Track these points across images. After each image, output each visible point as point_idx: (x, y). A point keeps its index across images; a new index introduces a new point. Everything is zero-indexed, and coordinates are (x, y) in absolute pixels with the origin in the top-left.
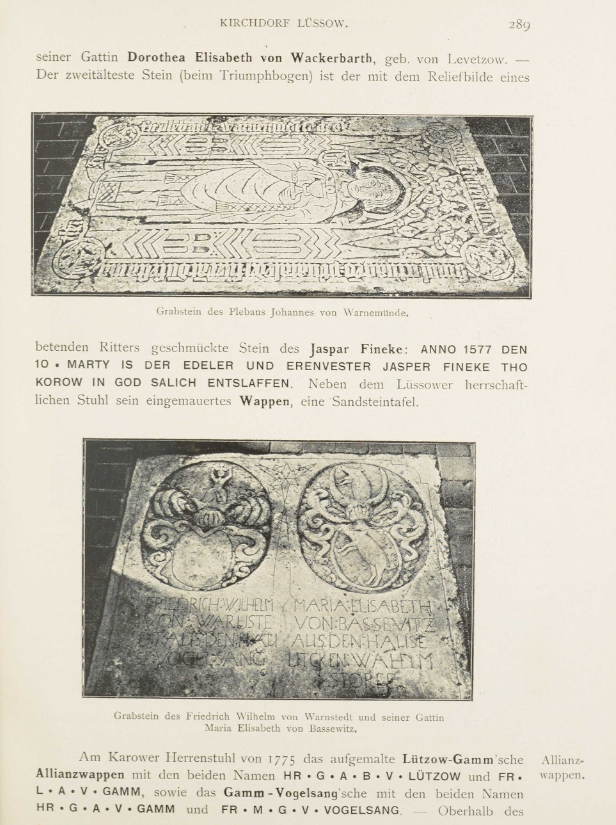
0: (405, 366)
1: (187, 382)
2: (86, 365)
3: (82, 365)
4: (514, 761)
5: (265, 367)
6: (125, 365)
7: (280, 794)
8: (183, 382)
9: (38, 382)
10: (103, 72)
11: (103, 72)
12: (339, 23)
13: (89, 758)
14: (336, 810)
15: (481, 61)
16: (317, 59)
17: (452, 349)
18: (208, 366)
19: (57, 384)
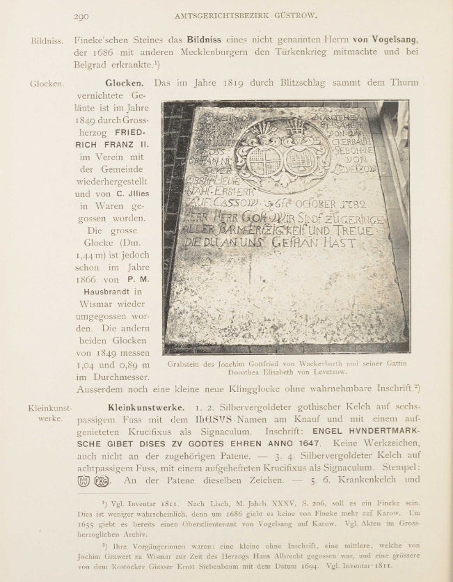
0: (154, 443)
2: (405, 431)
5: (367, 432)
6: (149, 444)
7: (375, 40)
10: (321, 387)
11: (321, 387)
12: (311, 15)
17: (290, 443)
18: (337, 432)
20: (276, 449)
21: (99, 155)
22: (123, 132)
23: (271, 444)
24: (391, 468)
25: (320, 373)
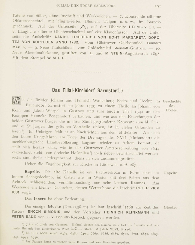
1: (92, 37)
2: (128, 38)
3: (127, 38)
4: (33, 32)
8: (91, 37)
9: (34, 42)
13: (35, 37)
14: (152, 38)
15: (61, 153)
16: (56, 207)
19: (129, 38)
20: (35, 44)
21: (86, 42)
22: (75, 37)
23: (57, 42)
24: (34, 58)
25: (150, 43)
